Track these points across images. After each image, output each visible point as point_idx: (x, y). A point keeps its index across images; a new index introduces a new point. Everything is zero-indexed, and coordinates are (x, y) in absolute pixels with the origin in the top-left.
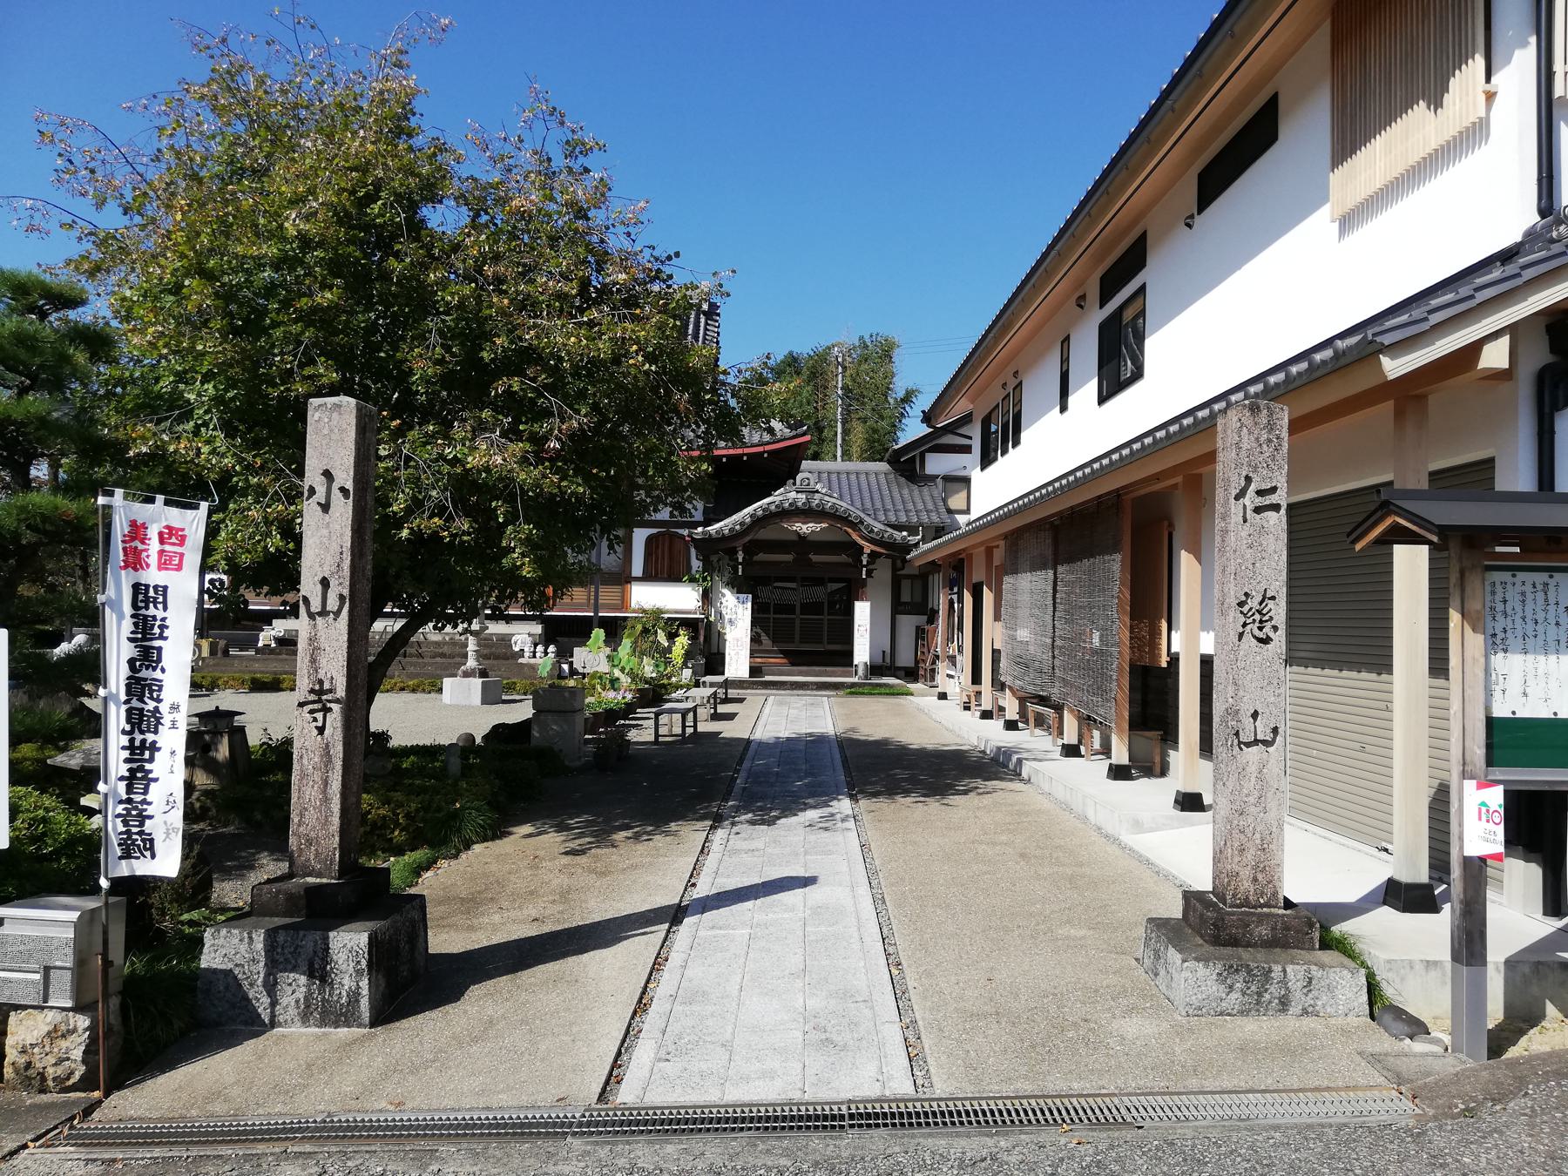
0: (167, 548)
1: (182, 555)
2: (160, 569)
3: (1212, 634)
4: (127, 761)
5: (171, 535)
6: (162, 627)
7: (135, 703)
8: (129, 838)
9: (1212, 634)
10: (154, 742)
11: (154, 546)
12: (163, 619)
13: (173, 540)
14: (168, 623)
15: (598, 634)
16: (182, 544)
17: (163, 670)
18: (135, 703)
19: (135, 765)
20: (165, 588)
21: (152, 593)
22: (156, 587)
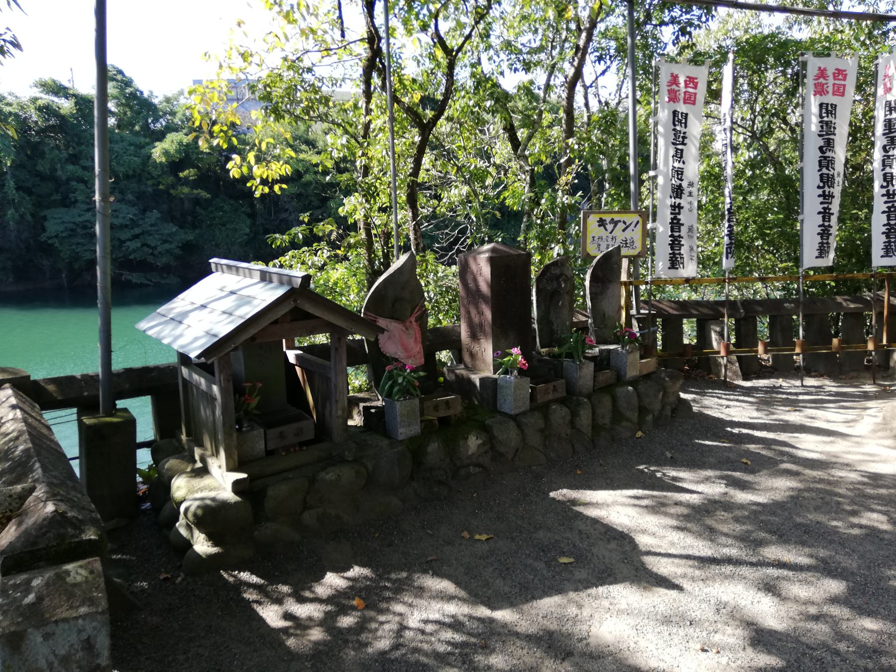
0: (837, 82)
1: (844, 86)
2: (834, 94)
3: (117, 402)
4: (886, 202)
5: (839, 74)
6: (684, 138)
7: (824, 171)
8: (674, 256)
9: (117, 402)
10: (679, 204)
11: (831, 81)
12: (684, 133)
13: (840, 77)
14: (687, 135)
15: (888, 170)
16: (844, 79)
17: (684, 163)
18: (824, 171)
19: (890, 205)
20: (687, 114)
21: (830, 108)
22: (832, 105)
